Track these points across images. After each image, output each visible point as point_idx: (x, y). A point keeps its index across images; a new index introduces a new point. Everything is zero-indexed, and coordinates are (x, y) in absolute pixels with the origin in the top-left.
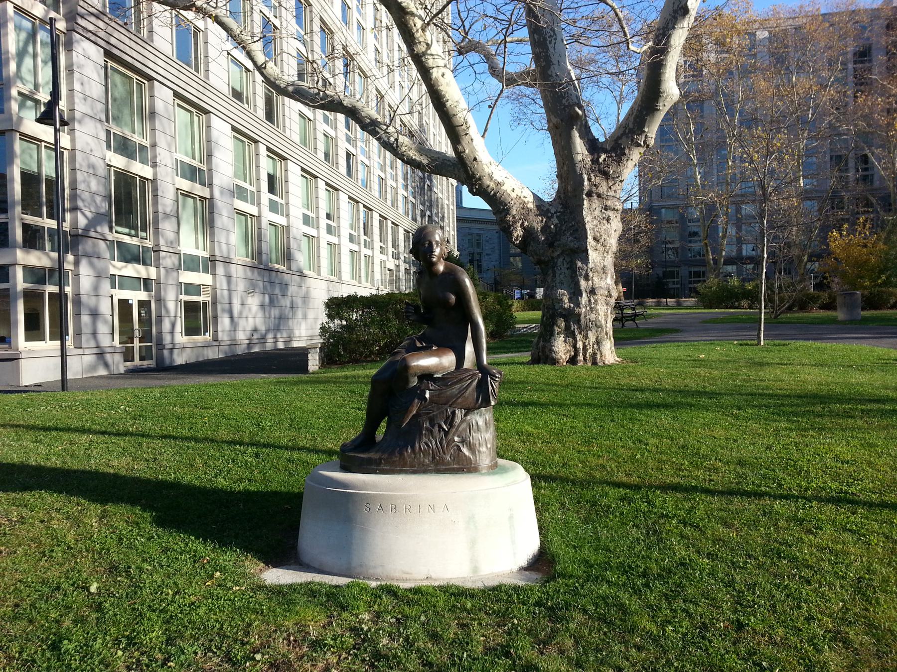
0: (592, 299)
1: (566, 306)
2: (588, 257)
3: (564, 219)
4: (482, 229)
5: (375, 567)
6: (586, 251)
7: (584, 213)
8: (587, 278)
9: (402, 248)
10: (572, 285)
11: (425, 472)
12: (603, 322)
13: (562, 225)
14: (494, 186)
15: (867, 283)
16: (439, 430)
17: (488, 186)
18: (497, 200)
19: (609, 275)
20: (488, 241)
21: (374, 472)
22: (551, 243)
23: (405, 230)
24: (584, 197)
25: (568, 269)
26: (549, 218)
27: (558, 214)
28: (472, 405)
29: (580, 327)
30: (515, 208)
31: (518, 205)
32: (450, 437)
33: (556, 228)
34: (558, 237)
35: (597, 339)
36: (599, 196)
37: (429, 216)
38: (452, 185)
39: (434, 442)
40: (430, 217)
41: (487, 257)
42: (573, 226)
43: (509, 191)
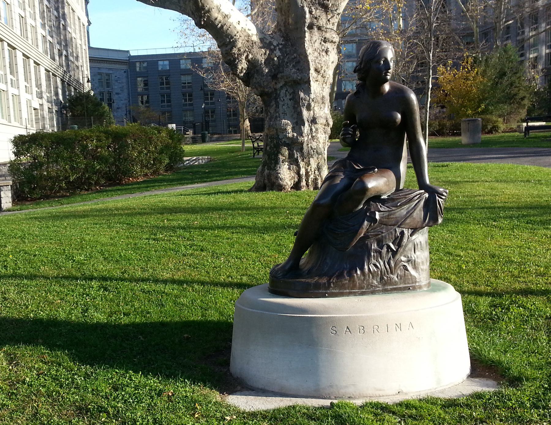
0: (313, 128)
1: (290, 135)
2: (310, 88)
3: (286, 51)
4: (110, 69)
5: (346, 387)
6: (309, 82)
7: (306, 45)
8: (309, 108)
9: (44, 88)
10: (295, 116)
11: (373, 293)
12: (322, 149)
13: (284, 57)
14: (221, 19)
15: (470, 112)
16: (388, 251)
17: (216, 19)
18: (223, 32)
19: (327, 105)
20: (117, 81)
21: (323, 296)
22: (274, 77)
23: (46, 70)
24: (306, 29)
25: (290, 100)
26: (272, 51)
27: (280, 46)
28: (419, 225)
29: (302, 155)
30: (240, 41)
31: (243, 37)
32: (397, 257)
33: (279, 60)
34: (281, 69)
35: (318, 165)
36: (319, 28)
37: (65, 56)
38: (84, 25)
39: (382, 263)
40: (67, 57)
41: (116, 96)
42: (295, 58)
43: (235, 24)
